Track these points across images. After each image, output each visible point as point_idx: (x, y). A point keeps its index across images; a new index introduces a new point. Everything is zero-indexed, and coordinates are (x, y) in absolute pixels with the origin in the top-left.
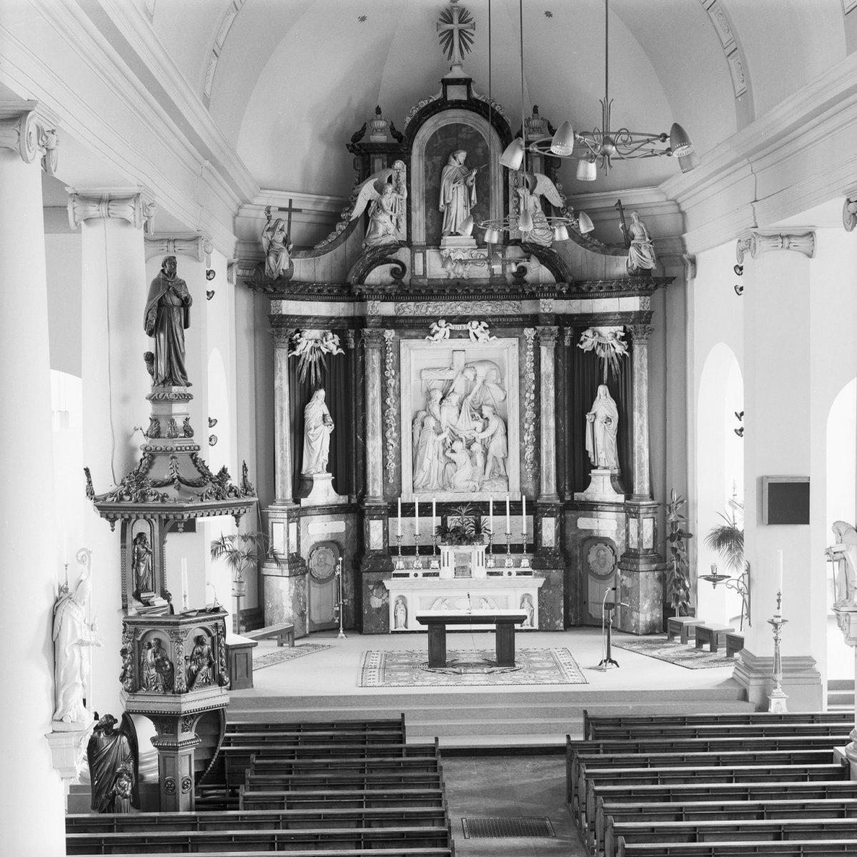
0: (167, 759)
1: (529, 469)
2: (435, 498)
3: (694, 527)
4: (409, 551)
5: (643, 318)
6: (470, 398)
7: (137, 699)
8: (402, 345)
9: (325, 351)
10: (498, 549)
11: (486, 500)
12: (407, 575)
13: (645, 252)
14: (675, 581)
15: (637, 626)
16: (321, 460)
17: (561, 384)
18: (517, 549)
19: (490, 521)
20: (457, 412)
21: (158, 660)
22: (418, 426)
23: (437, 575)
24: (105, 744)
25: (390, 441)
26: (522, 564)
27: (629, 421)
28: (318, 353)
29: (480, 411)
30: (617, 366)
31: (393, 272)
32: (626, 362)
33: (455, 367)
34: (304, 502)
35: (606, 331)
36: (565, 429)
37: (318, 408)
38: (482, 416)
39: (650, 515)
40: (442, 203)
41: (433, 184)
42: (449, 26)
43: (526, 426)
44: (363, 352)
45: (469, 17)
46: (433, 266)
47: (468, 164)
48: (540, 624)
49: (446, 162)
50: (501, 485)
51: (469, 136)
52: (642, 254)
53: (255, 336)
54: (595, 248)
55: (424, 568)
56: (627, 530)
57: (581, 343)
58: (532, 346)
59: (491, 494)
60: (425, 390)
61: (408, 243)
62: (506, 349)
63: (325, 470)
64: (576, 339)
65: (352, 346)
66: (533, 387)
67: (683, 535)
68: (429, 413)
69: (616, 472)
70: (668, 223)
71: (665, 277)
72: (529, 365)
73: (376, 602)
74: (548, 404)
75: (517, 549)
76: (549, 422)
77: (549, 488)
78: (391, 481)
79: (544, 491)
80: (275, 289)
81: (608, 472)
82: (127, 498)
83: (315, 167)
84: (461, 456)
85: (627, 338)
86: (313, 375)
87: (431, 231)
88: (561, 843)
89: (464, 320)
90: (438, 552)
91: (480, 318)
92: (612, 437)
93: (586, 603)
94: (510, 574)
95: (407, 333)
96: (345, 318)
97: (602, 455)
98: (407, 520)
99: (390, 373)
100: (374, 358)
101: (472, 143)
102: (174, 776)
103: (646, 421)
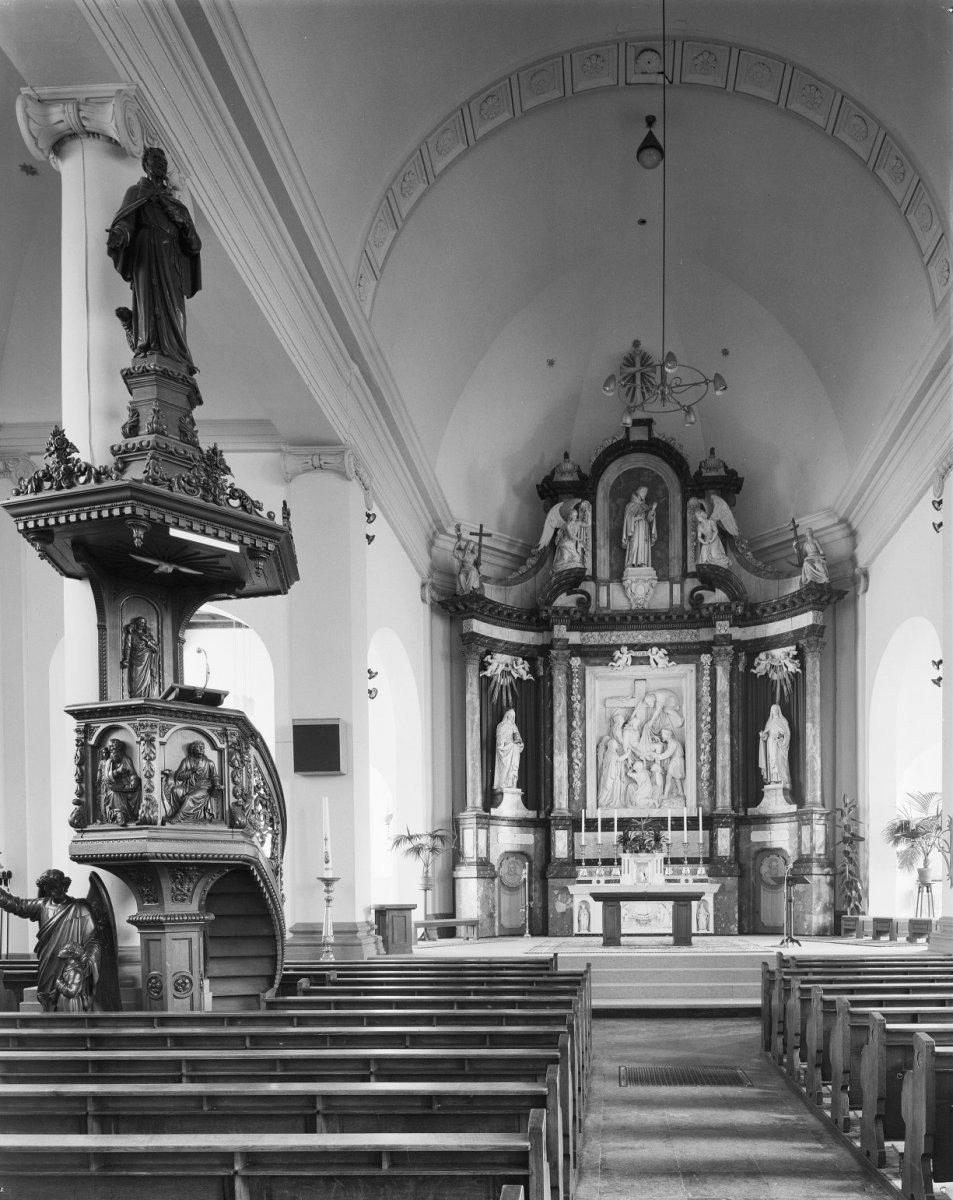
0: (152, 944)
1: (705, 785)
2: (616, 814)
3: (865, 832)
4: (591, 862)
5: (814, 630)
6: (650, 723)
7: (87, 836)
8: (587, 672)
9: (516, 676)
10: (677, 861)
11: (663, 816)
12: (590, 882)
13: (818, 566)
14: (848, 882)
15: (809, 926)
16: (511, 775)
17: (735, 707)
18: (693, 861)
19: (669, 835)
20: (638, 735)
21: (118, 773)
22: (602, 748)
23: (618, 881)
24: (50, 916)
25: (576, 761)
26: (699, 872)
27: (801, 734)
28: (509, 679)
29: (659, 734)
30: (790, 686)
31: (579, 602)
32: (798, 680)
33: (637, 696)
34: (494, 812)
35: (778, 653)
36: (739, 748)
37: (508, 728)
38: (661, 739)
39: (822, 822)
40: (624, 537)
41: (616, 524)
42: (632, 370)
43: (703, 746)
44: (551, 679)
45: (650, 362)
46: (615, 599)
47: (648, 500)
48: (715, 928)
49: (629, 500)
50: (678, 802)
51: (650, 479)
52: (815, 568)
53: (451, 662)
54: (769, 575)
55: (606, 875)
56: (800, 837)
57: (755, 668)
58: (708, 672)
59: (669, 813)
60: (608, 716)
61: (594, 578)
62: (683, 676)
63: (515, 784)
64: (750, 665)
65: (542, 673)
66: (709, 710)
67: (854, 839)
68: (611, 734)
69: (788, 786)
70: (840, 548)
71: (837, 594)
72: (705, 689)
73: (560, 907)
74: (724, 722)
75: (693, 861)
76: (724, 738)
77: (724, 801)
78: (577, 798)
79: (719, 803)
80: (466, 607)
81: (781, 786)
82: (47, 485)
83: (511, 518)
84: (641, 775)
85: (800, 656)
86: (504, 697)
87: (614, 568)
88: (764, 1093)
89: (645, 647)
90: (619, 862)
91: (660, 646)
92: (784, 753)
93: (758, 912)
94: (687, 881)
95: (592, 661)
96: (535, 646)
97: (774, 770)
98: (591, 835)
99: (576, 697)
100: (560, 679)
101: (655, 485)
102: (161, 971)
103: (818, 731)
